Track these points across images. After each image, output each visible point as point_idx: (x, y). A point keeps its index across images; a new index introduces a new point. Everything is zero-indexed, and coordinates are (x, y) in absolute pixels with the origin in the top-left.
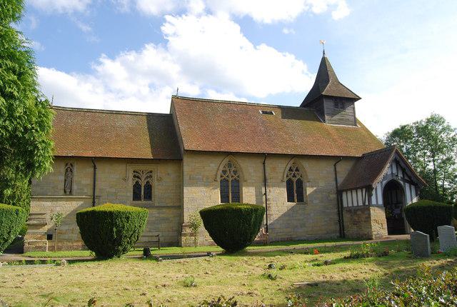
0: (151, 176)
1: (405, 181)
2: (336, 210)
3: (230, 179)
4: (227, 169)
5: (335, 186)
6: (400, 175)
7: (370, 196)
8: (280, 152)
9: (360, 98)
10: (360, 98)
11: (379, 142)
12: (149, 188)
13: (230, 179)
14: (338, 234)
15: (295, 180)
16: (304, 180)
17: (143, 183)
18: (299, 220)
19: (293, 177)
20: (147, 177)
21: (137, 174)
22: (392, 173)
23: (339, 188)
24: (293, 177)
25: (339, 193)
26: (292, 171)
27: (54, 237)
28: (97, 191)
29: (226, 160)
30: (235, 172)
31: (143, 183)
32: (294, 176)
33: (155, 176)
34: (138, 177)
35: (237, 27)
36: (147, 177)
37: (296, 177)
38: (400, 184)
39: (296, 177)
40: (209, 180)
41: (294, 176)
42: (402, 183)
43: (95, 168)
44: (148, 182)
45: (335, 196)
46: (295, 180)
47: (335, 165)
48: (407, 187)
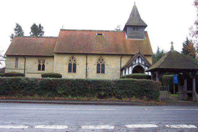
3: (72, 63)
4: (71, 59)
9: (40, 24)
10: (40, 24)
11: (152, 53)
12: (44, 66)
13: (72, 63)
15: (101, 64)
17: (41, 64)
19: (100, 63)
20: (43, 62)
21: (40, 61)
22: (139, 62)
24: (100, 63)
25: (122, 70)
26: (100, 60)
30: (75, 61)
31: (41, 64)
32: (101, 62)
33: (46, 62)
35: (157, 51)
36: (43, 62)
41: (101, 62)
42: (144, 67)
43: (87, 57)
44: (43, 64)
46: (101, 64)
47: (121, 58)
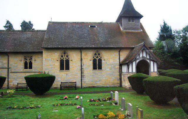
0: (32, 59)
1: (150, 60)
2: (119, 73)
3: (65, 59)
4: (63, 55)
5: (119, 62)
6: (148, 57)
7: (128, 68)
8: (76, 46)
14: (119, 85)
15: (97, 59)
16: (103, 59)
17: (28, 61)
18: (98, 78)
19: (96, 58)
21: (26, 58)
22: (143, 56)
23: (121, 63)
24: (96, 58)
25: (121, 65)
27: (97, 71)
28: (9, 65)
29: (96, 51)
30: (67, 56)
31: (28, 61)
32: (97, 57)
33: (33, 58)
34: (27, 59)
37: (98, 58)
38: (147, 62)
39: (98, 58)
40: (54, 60)
41: (97, 57)
42: (149, 61)
45: (119, 67)
47: (119, 52)
48: (152, 63)
